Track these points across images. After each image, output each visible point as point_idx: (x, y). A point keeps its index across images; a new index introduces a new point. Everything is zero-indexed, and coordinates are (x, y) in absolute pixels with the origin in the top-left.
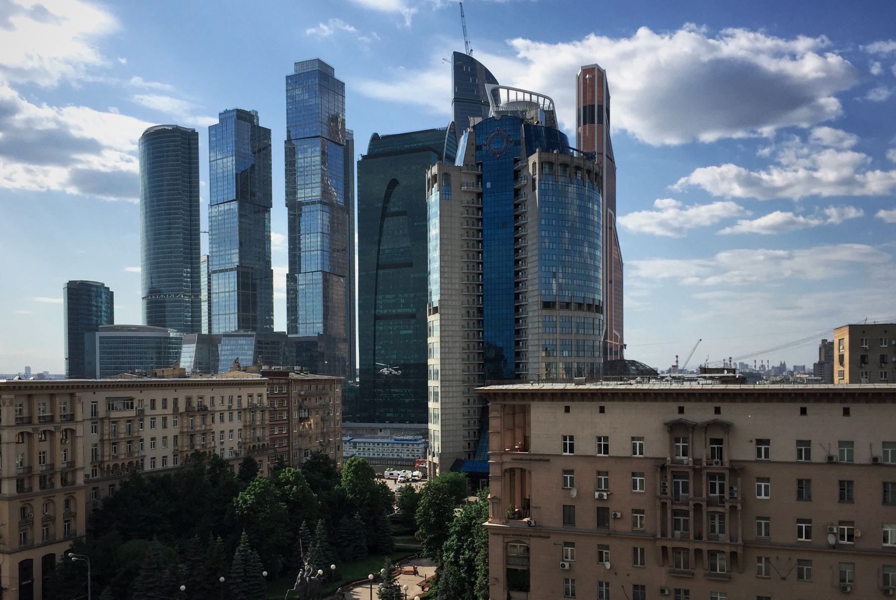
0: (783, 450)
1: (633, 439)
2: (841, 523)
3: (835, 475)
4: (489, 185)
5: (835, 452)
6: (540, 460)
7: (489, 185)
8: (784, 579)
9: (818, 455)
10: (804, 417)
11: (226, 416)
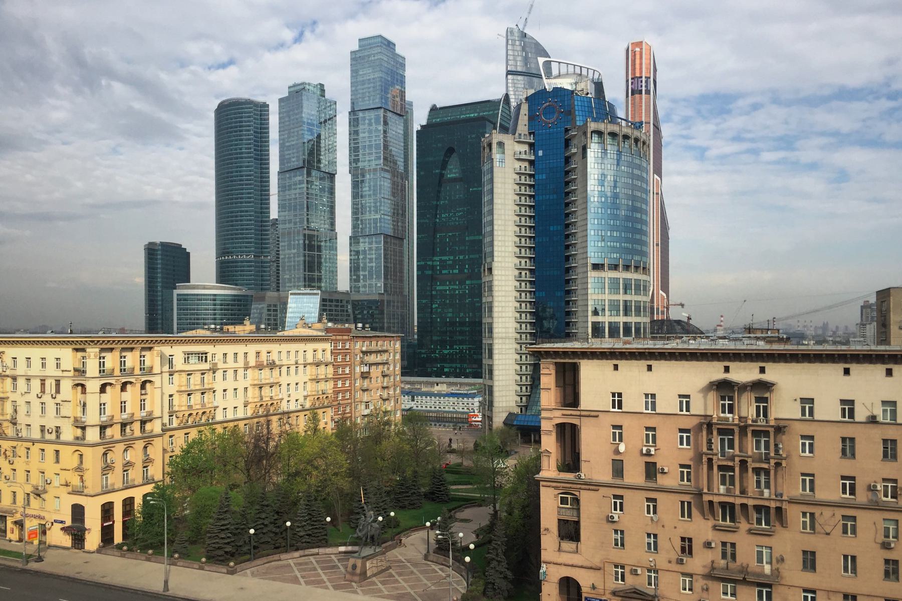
0: (828, 409)
1: (680, 396)
2: (884, 480)
3: (877, 434)
4: (540, 153)
5: (878, 411)
6: (589, 416)
7: (540, 153)
8: (828, 534)
9: (861, 414)
10: (847, 378)
11: (293, 369)
